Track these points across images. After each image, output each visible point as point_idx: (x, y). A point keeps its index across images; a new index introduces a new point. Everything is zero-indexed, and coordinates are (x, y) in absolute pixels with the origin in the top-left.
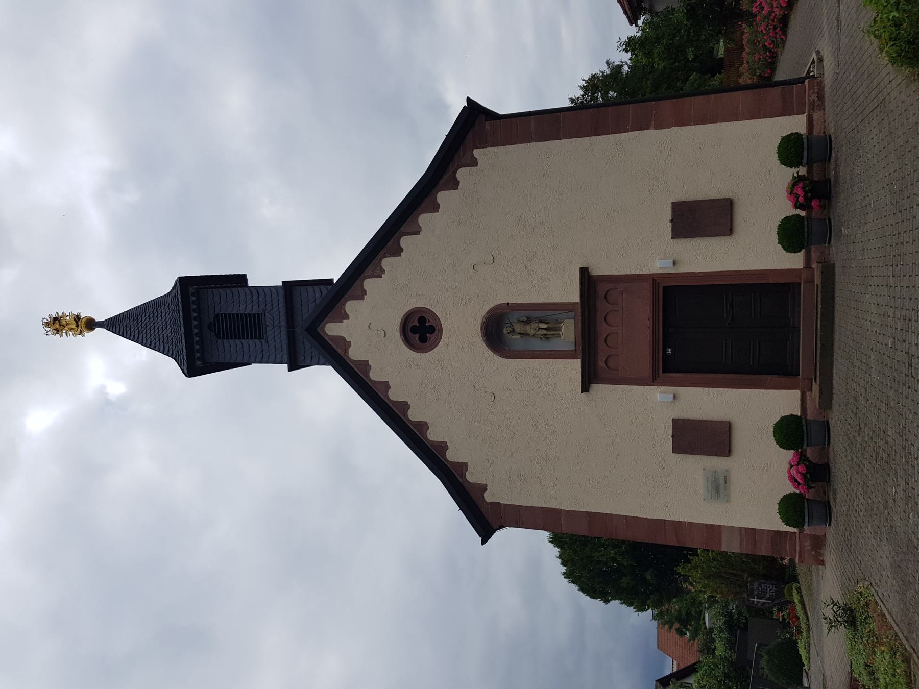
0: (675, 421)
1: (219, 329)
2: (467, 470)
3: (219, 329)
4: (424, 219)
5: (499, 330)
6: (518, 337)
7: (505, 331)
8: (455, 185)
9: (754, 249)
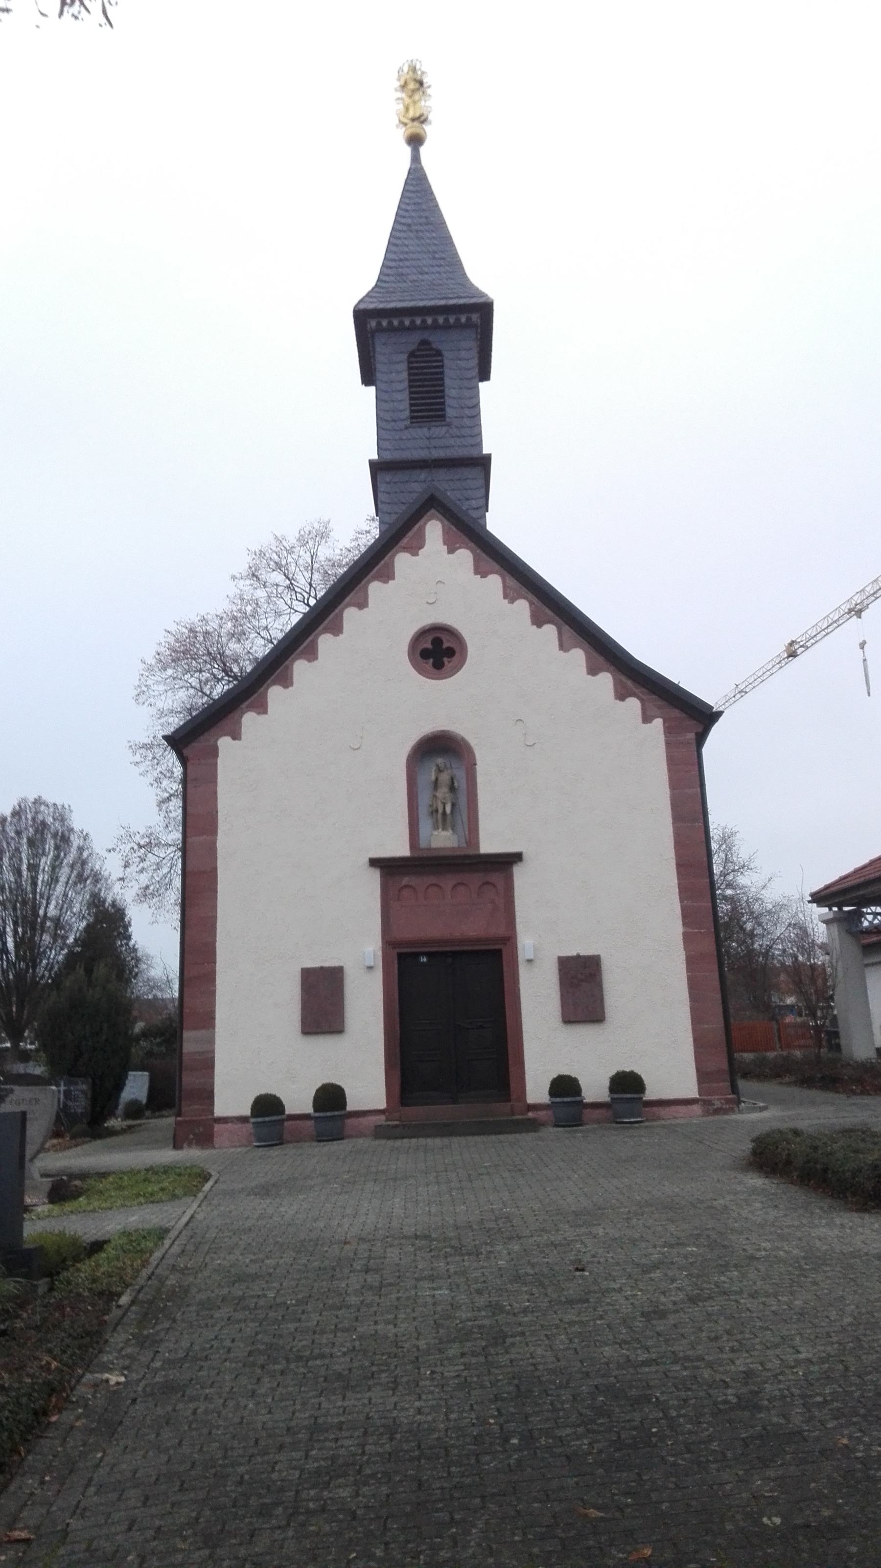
1: (423, 356)
2: (259, 713)
3: (423, 356)
5: (440, 754)
6: (433, 778)
8: (621, 696)
9: (549, 1049)
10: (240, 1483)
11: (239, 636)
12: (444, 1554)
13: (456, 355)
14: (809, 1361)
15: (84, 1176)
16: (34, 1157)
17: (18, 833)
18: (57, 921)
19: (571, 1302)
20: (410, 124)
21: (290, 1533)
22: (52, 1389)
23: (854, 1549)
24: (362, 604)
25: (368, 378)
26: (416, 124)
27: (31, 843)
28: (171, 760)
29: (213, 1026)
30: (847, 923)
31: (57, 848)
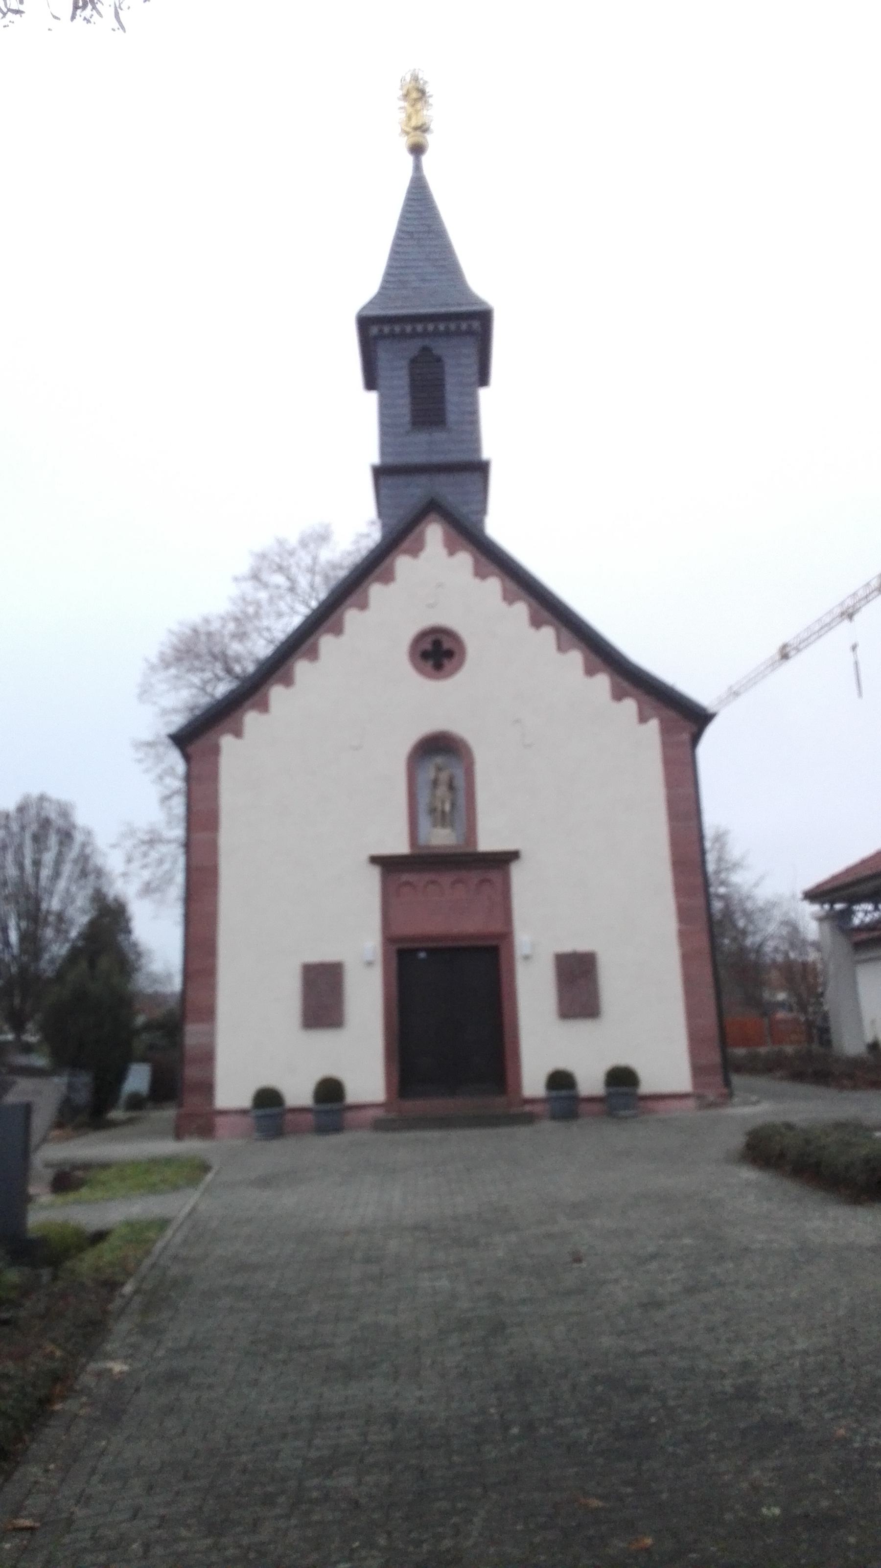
5: (439, 753)
9: (545, 1044)
10: (244, 1471)
11: (241, 636)
12: (447, 1543)
13: (456, 361)
14: (805, 1353)
15: (87, 1166)
16: (38, 1147)
17: (23, 828)
18: (60, 917)
19: (568, 1293)
20: (412, 134)
21: (294, 1521)
22: (57, 1378)
23: (852, 1540)
24: (363, 606)
25: (370, 383)
26: (418, 133)
27: (36, 838)
28: (175, 760)
30: (839, 921)
31: (61, 843)
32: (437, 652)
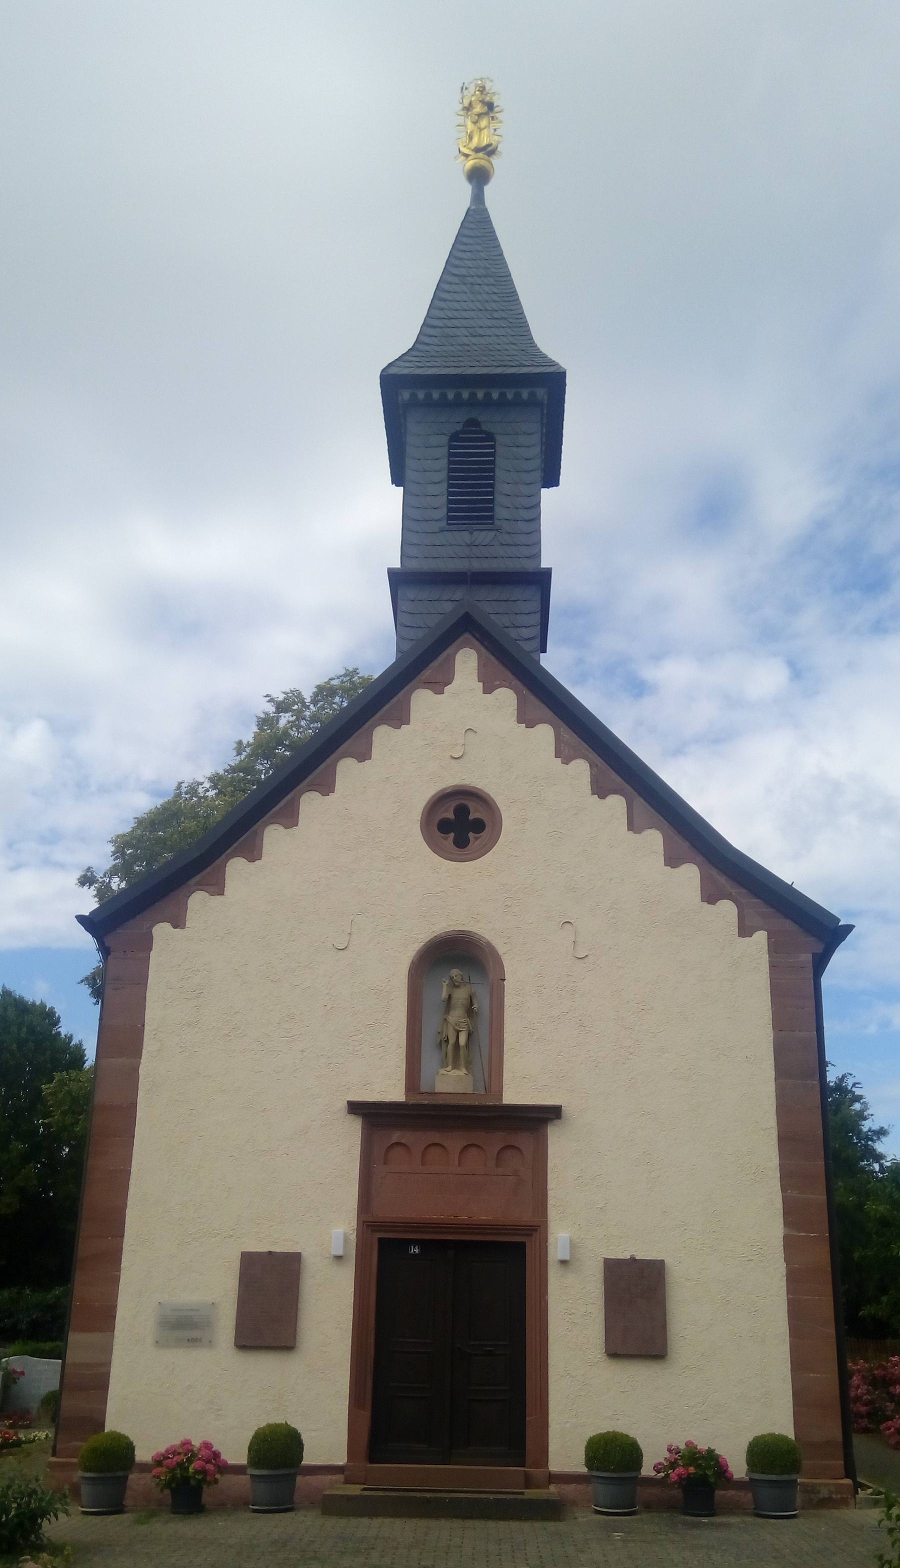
0: (296, 1258)
2: (212, 894)
4: (654, 840)
5: (455, 963)
6: (444, 995)
7: (455, 972)
8: (710, 896)
9: (583, 1395)
13: (515, 446)
24: (364, 755)
29: (112, 1328)
32: (460, 822)
